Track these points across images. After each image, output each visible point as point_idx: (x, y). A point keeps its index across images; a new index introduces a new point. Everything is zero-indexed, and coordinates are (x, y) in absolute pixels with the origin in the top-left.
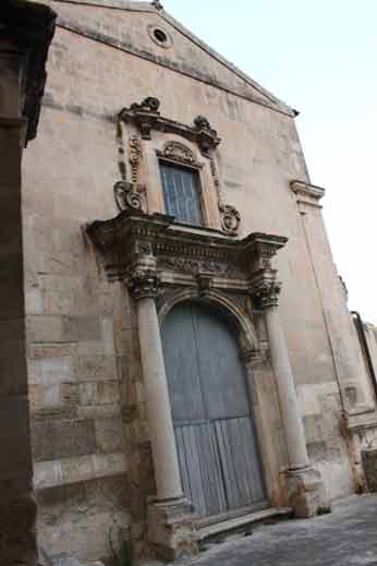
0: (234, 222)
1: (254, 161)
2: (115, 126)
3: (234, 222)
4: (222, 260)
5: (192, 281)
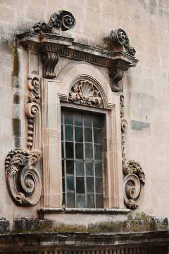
2: (10, 57)
3: (137, 186)
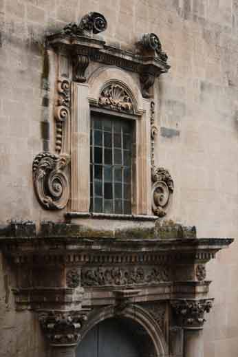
0: (166, 194)
1: (202, 87)
2: (40, 58)
3: (166, 194)
4: (148, 263)
5: (109, 299)
